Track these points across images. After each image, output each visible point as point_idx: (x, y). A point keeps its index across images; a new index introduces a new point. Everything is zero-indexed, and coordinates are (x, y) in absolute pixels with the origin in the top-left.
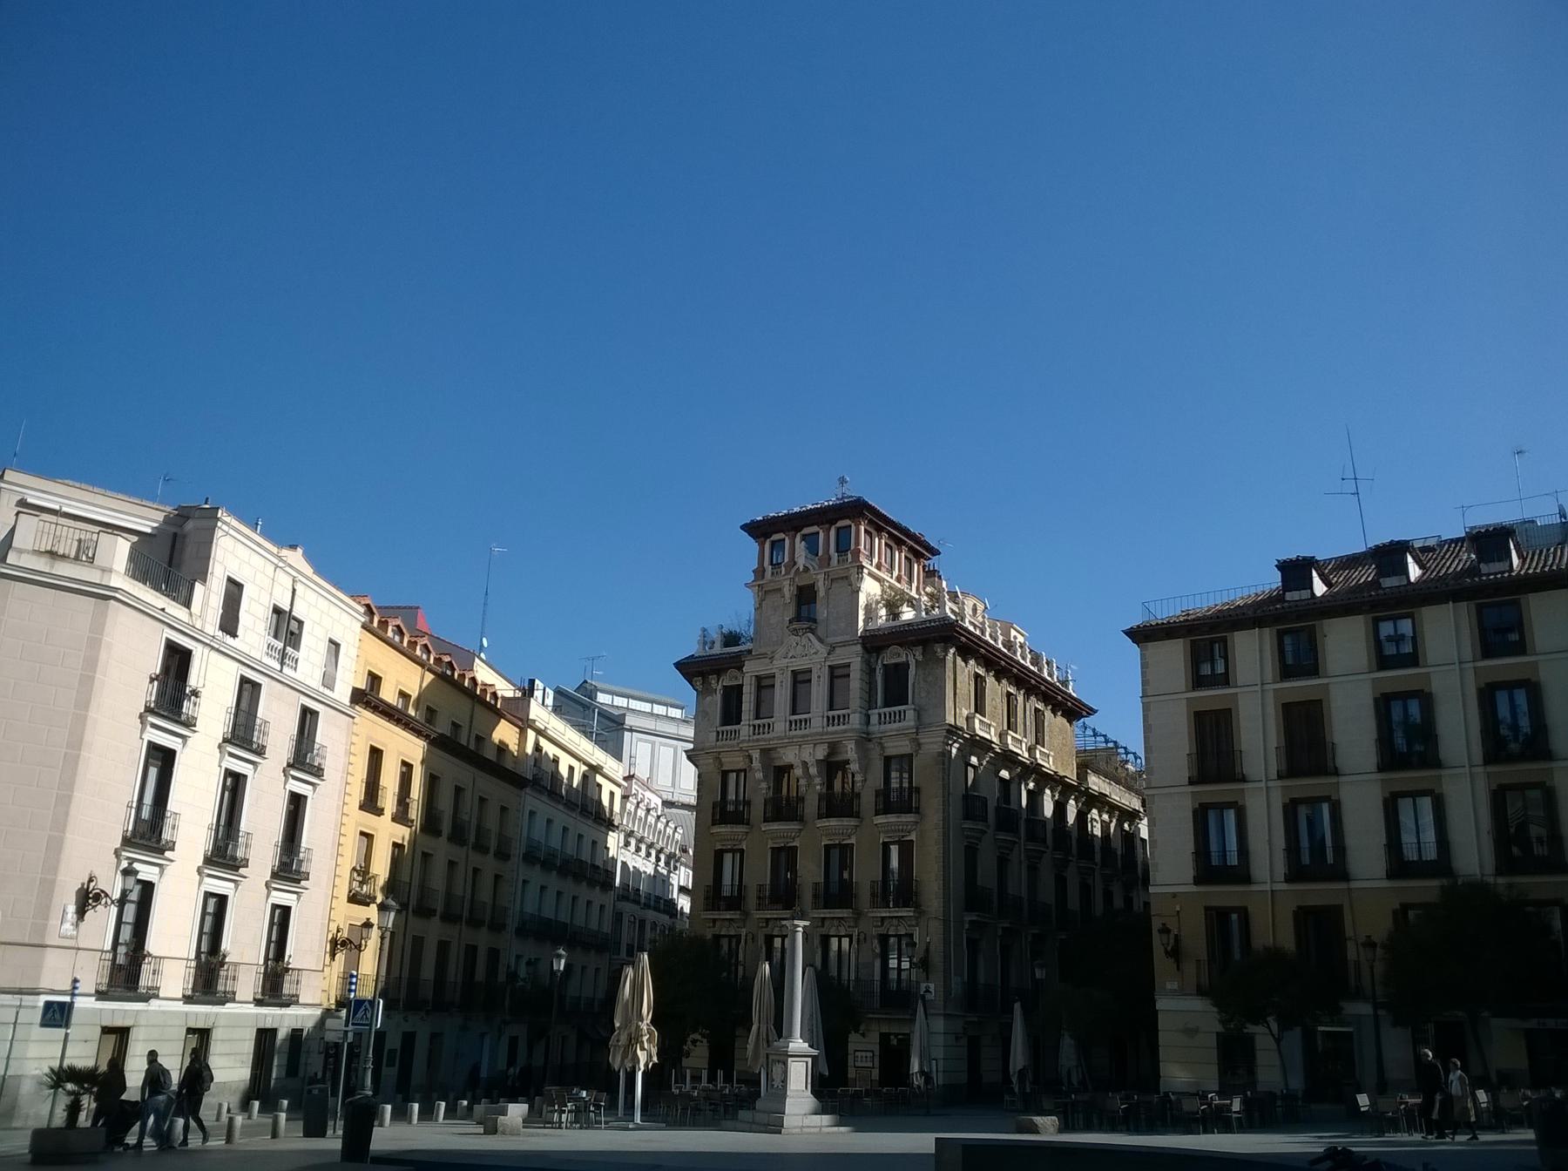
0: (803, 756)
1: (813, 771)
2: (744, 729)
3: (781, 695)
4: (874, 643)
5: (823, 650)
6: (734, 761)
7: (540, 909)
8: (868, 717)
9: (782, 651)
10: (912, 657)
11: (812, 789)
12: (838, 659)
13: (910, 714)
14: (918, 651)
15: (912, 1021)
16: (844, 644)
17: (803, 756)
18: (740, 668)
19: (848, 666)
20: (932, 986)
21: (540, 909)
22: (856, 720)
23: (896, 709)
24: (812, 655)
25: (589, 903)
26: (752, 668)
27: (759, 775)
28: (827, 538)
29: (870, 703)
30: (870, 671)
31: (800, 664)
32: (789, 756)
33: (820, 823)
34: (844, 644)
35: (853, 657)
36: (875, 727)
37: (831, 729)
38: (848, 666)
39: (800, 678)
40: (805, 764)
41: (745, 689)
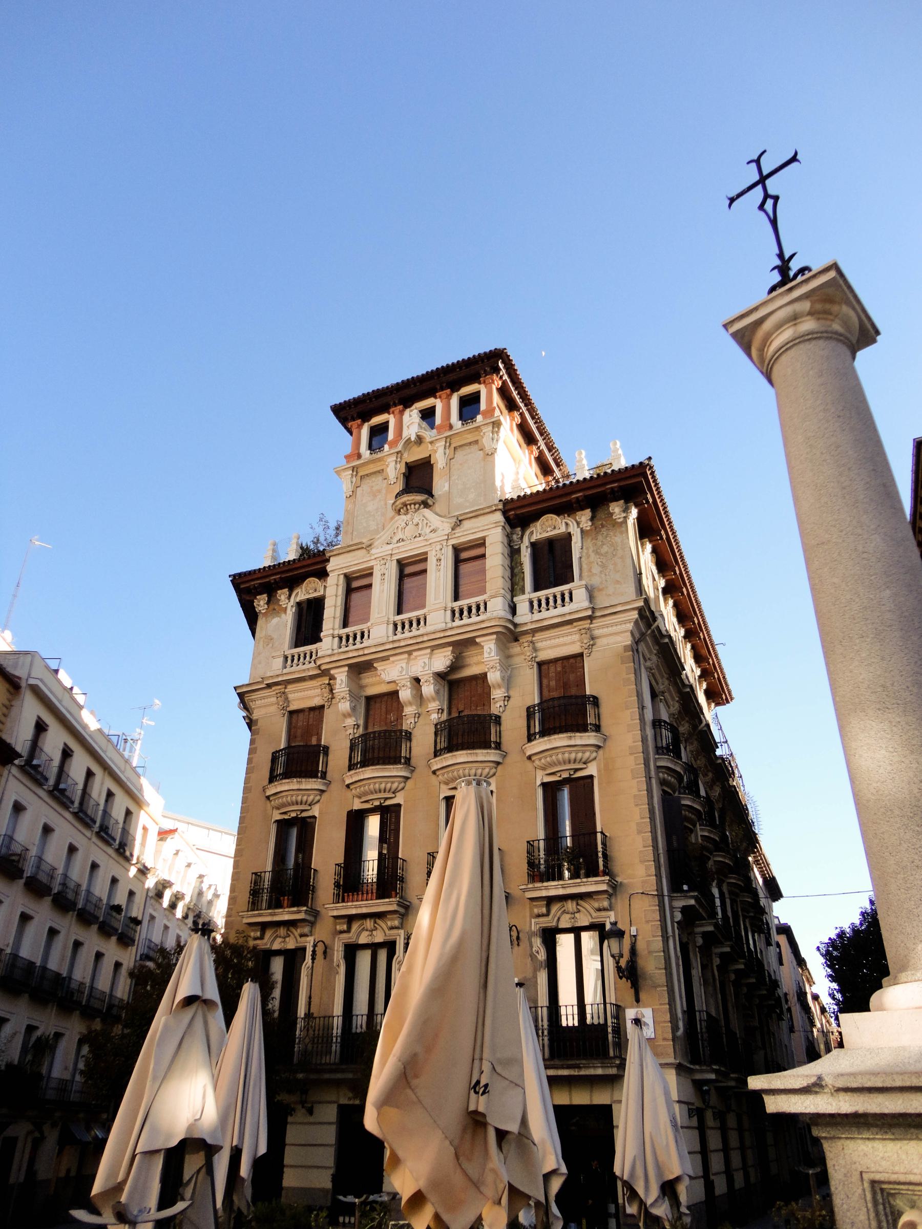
0: (411, 673)
1: (428, 689)
2: (327, 646)
3: (383, 591)
4: (519, 513)
5: (444, 526)
6: (305, 696)
7: (287, 1166)
9: (385, 536)
10: (575, 526)
11: (423, 719)
12: (468, 533)
13: (580, 595)
14: (584, 516)
15: (615, 1080)
16: (476, 515)
17: (411, 673)
18: (322, 574)
19: (481, 543)
20: (647, 1014)
21: (287, 1166)
22: (497, 607)
23: (557, 590)
24: (430, 533)
25: (99, 956)
26: (337, 566)
27: (345, 706)
28: (447, 406)
29: (515, 587)
30: (513, 553)
31: (408, 550)
32: (392, 674)
33: (437, 763)
35: (493, 531)
36: (524, 615)
37: (458, 622)
38: (481, 543)
39: (409, 570)
41: (328, 603)
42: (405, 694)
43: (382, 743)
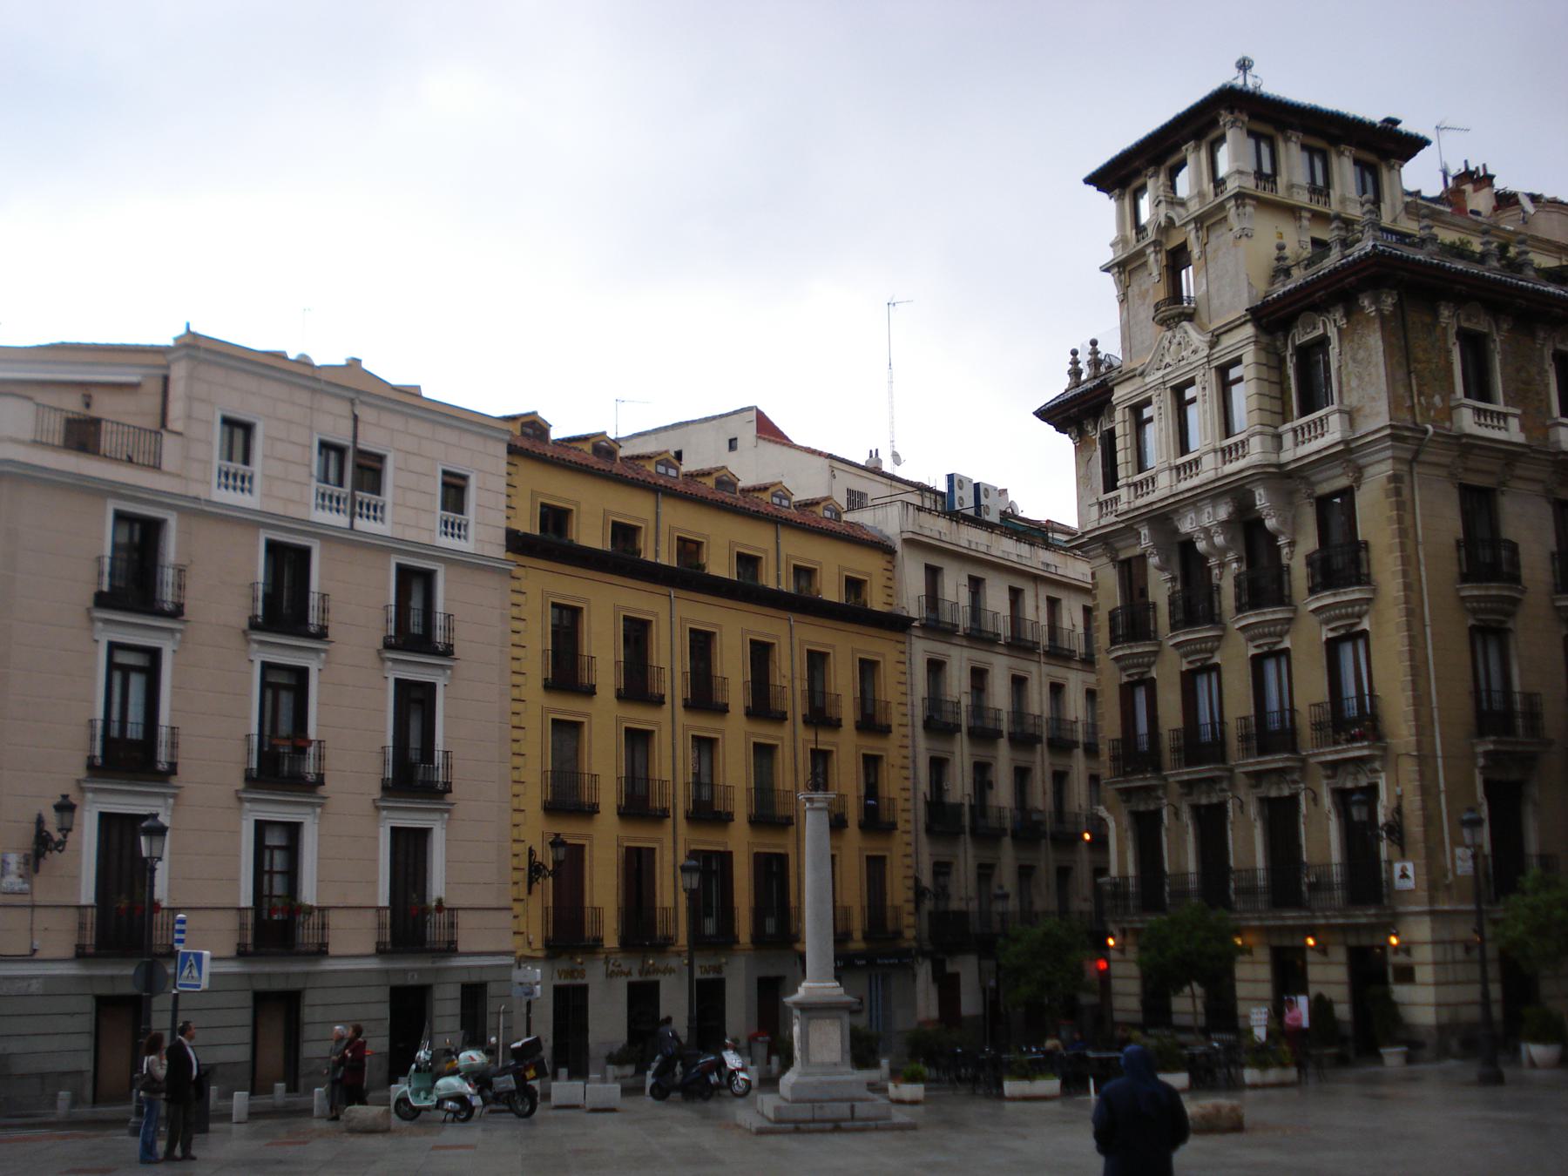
1: (1219, 540)
8: (1278, 437)
32: (1187, 525)
34: (1230, 328)
40: (1206, 530)
42: (1201, 546)
43: (1196, 604)
